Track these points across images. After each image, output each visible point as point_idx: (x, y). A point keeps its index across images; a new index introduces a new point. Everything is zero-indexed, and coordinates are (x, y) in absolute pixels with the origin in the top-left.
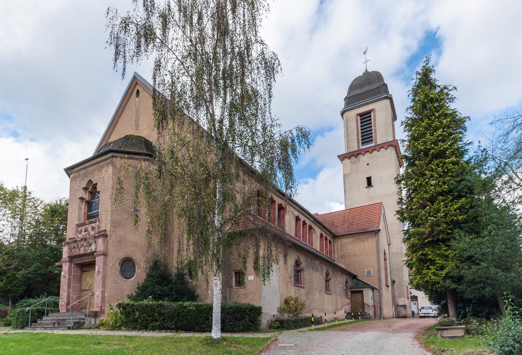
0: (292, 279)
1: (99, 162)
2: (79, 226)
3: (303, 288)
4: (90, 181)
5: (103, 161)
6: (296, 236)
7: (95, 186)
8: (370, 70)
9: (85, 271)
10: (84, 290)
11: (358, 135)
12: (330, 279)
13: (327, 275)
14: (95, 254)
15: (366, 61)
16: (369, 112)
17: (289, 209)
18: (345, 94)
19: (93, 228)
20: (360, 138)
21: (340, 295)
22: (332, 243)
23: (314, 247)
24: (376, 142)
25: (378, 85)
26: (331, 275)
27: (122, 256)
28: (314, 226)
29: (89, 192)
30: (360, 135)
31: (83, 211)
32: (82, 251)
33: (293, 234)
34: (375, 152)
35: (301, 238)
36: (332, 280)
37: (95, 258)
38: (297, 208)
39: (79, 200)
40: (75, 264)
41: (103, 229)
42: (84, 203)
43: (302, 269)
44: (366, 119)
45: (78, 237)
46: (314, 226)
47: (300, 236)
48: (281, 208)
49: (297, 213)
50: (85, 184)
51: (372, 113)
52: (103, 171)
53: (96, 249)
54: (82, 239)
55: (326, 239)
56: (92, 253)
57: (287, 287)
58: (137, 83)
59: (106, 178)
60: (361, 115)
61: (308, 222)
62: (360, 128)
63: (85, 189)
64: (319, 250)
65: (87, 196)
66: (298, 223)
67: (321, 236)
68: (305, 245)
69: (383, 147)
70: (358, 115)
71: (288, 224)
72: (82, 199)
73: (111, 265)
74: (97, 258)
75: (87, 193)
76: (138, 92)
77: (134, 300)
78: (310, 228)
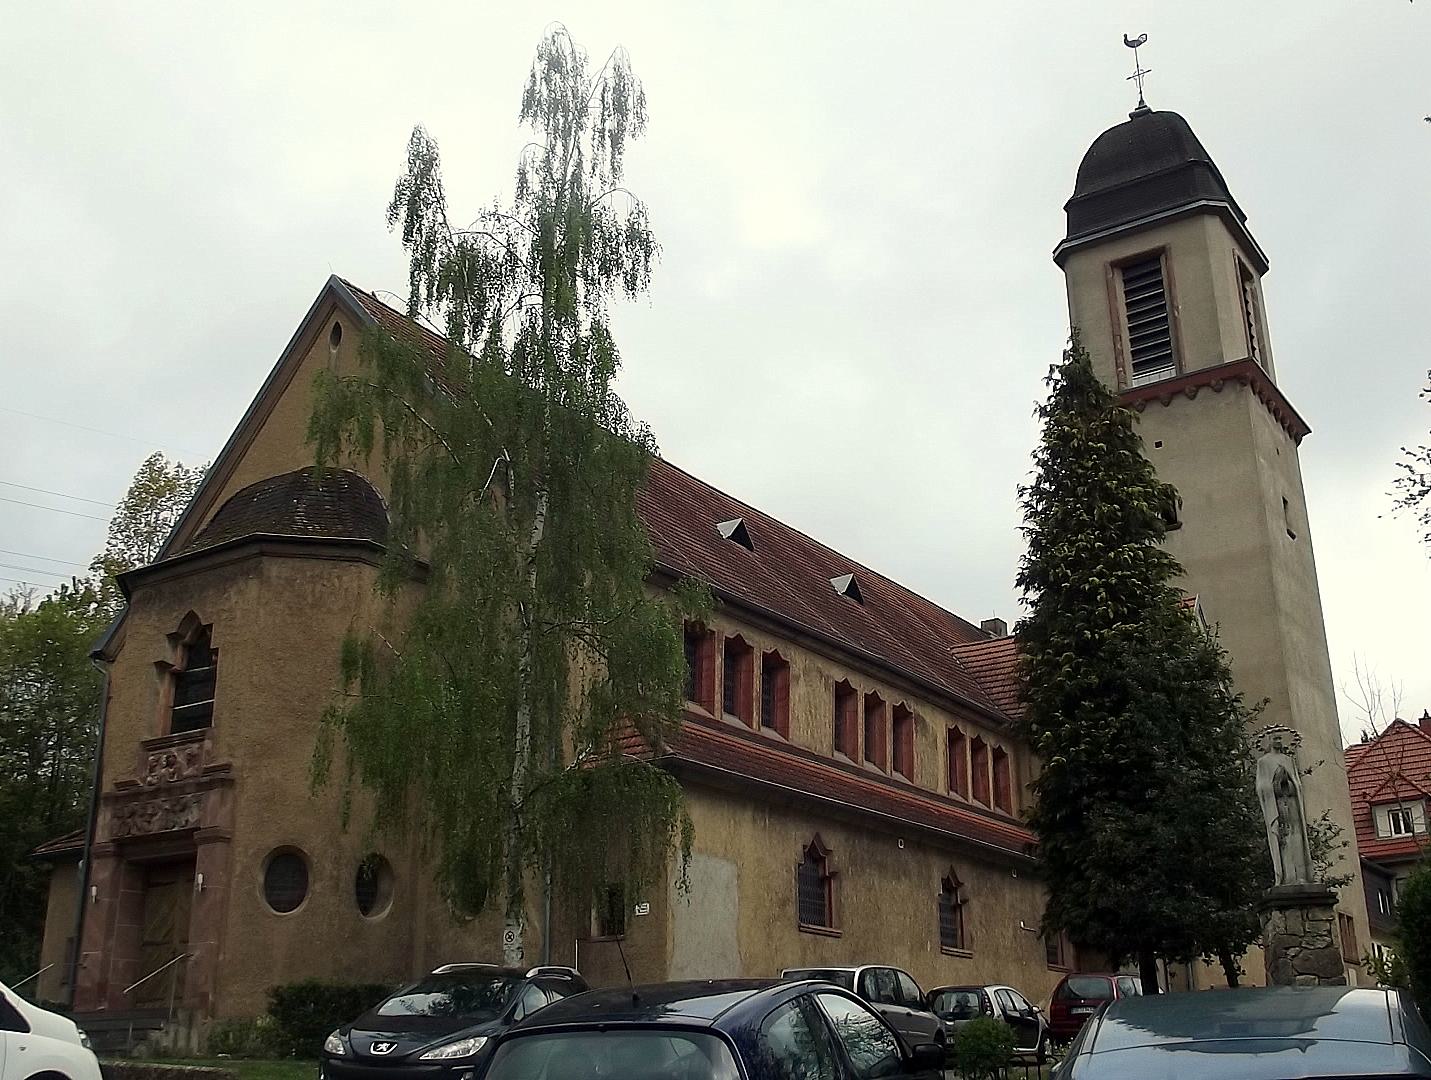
0: (792, 910)
1: (222, 565)
2: (150, 746)
3: (837, 936)
4: (191, 617)
5: (232, 562)
6: (838, 747)
7: (204, 632)
8: (1155, 107)
9: (158, 885)
10: (151, 944)
11: (1116, 337)
12: (965, 901)
13: (950, 886)
14: (196, 835)
15: (1139, 74)
16: (1155, 257)
17: (798, 660)
18: (1068, 192)
19: (192, 759)
20: (1128, 348)
21: (1019, 960)
22: (1010, 759)
23: (917, 783)
24: (1180, 368)
25: (1176, 161)
26: (968, 885)
27: (272, 842)
28: (913, 707)
29: (185, 646)
30: (1126, 336)
31: (162, 701)
32: (155, 827)
33: (824, 744)
34: (1180, 403)
35: (861, 755)
36: (975, 905)
37: (195, 846)
38: (839, 656)
39: (154, 669)
40: (130, 863)
41: (221, 761)
42: (167, 677)
43: (834, 875)
44: (1143, 277)
45: (144, 780)
46: (913, 707)
47: (855, 751)
48: (774, 666)
49: (838, 675)
50: (177, 623)
51: (1163, 258)
52: (232, 592)
53: (199, 821)
54: (158, 790)
55: (978, 747)
56: (188, 834)
57: (769, 936)
58: (334, 307)
59: (239, 614)
60: (1126, 266)
61: (890, 698)
62: (1123, 312)
63: (173, 638)
64: (942, 790)
65: (175, 658)
66: (849, 705)
67: (954, 737)
68: (876, 778)
69: (1208, 385)
70: (1115, 265)
71: (802, 718)
72: (162, 666)
73: (238, 869)
74: (200, 850)
75: (179, 648)
76: (337, 329)
77: (1063, 520)
78: (901, 715)
